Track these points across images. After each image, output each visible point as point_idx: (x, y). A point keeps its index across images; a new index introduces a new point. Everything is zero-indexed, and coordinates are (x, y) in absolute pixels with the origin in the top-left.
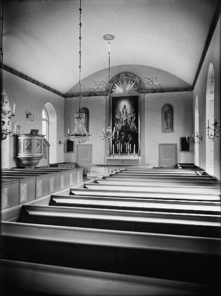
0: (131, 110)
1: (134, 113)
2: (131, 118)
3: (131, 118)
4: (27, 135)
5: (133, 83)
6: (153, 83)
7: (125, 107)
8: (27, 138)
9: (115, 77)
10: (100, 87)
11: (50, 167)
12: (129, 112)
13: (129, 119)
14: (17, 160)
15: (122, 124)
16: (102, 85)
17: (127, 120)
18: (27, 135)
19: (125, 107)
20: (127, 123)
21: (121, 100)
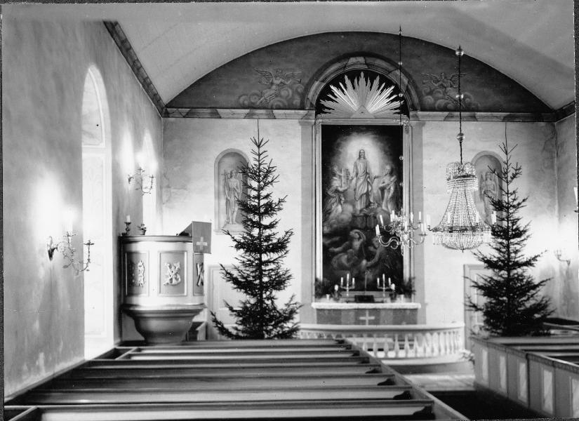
0: (383, 168)
1: (391, 174)
2: (382, 189)
3: (382, 189)
4: (170, 240)
5: (386, 87)
6: (445, 93)
7: (361, 155)
8: (171, 247)
9: (124, 34)
10: (284, 93)
11: (370, 324)
12: (375, 169)
13: (375, 191)
14: (125, 310)
15: (354, 206)
16: (291, 87)
17: (367, 194)
18: (170, 240)
19: (361, 155)
20: (368, 205)
21: (353, 131)
